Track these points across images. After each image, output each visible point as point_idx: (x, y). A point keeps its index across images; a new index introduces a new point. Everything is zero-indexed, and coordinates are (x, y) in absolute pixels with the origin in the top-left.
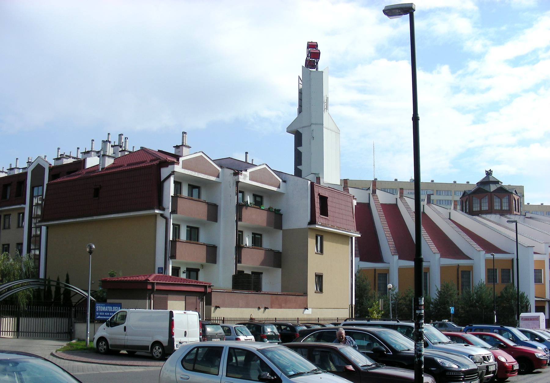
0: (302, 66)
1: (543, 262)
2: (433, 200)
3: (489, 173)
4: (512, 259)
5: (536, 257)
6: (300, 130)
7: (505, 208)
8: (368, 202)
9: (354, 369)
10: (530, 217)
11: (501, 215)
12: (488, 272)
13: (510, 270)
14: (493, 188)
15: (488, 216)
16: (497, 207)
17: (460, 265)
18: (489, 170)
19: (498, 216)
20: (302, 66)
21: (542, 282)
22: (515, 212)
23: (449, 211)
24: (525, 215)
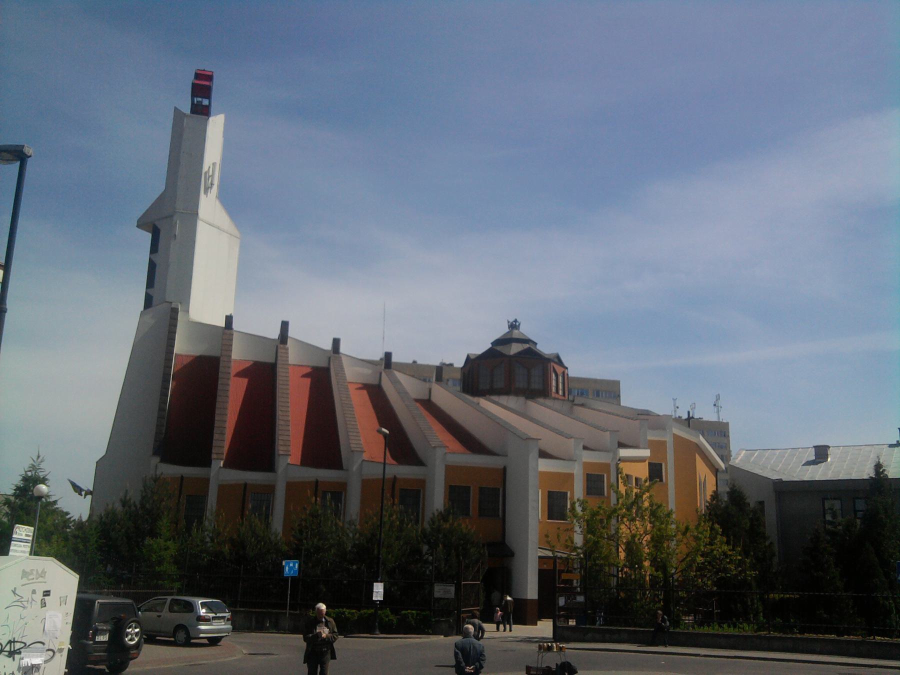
0: (175, 107)
1: (569, 477)
2: (454, 385)
3: (514, 326)
4: (502, 467)
5: (545, 465)
6: (157, 223)
7: (536, 385)
8: (272, 361)
9: (695, 456)
10: (203, 69)
11: (527, 398)
12: (587, 480)
13: (499, 489)
14: (515, 349)
15: (503, 399)
16: (520, 383)
17: (398, 476)
18: (513, 320)
19: (522, 399)
20: (175, 107)
21: (604, 494)
22: (553, 395)
23: (427, 385)
24: (573, 401)
